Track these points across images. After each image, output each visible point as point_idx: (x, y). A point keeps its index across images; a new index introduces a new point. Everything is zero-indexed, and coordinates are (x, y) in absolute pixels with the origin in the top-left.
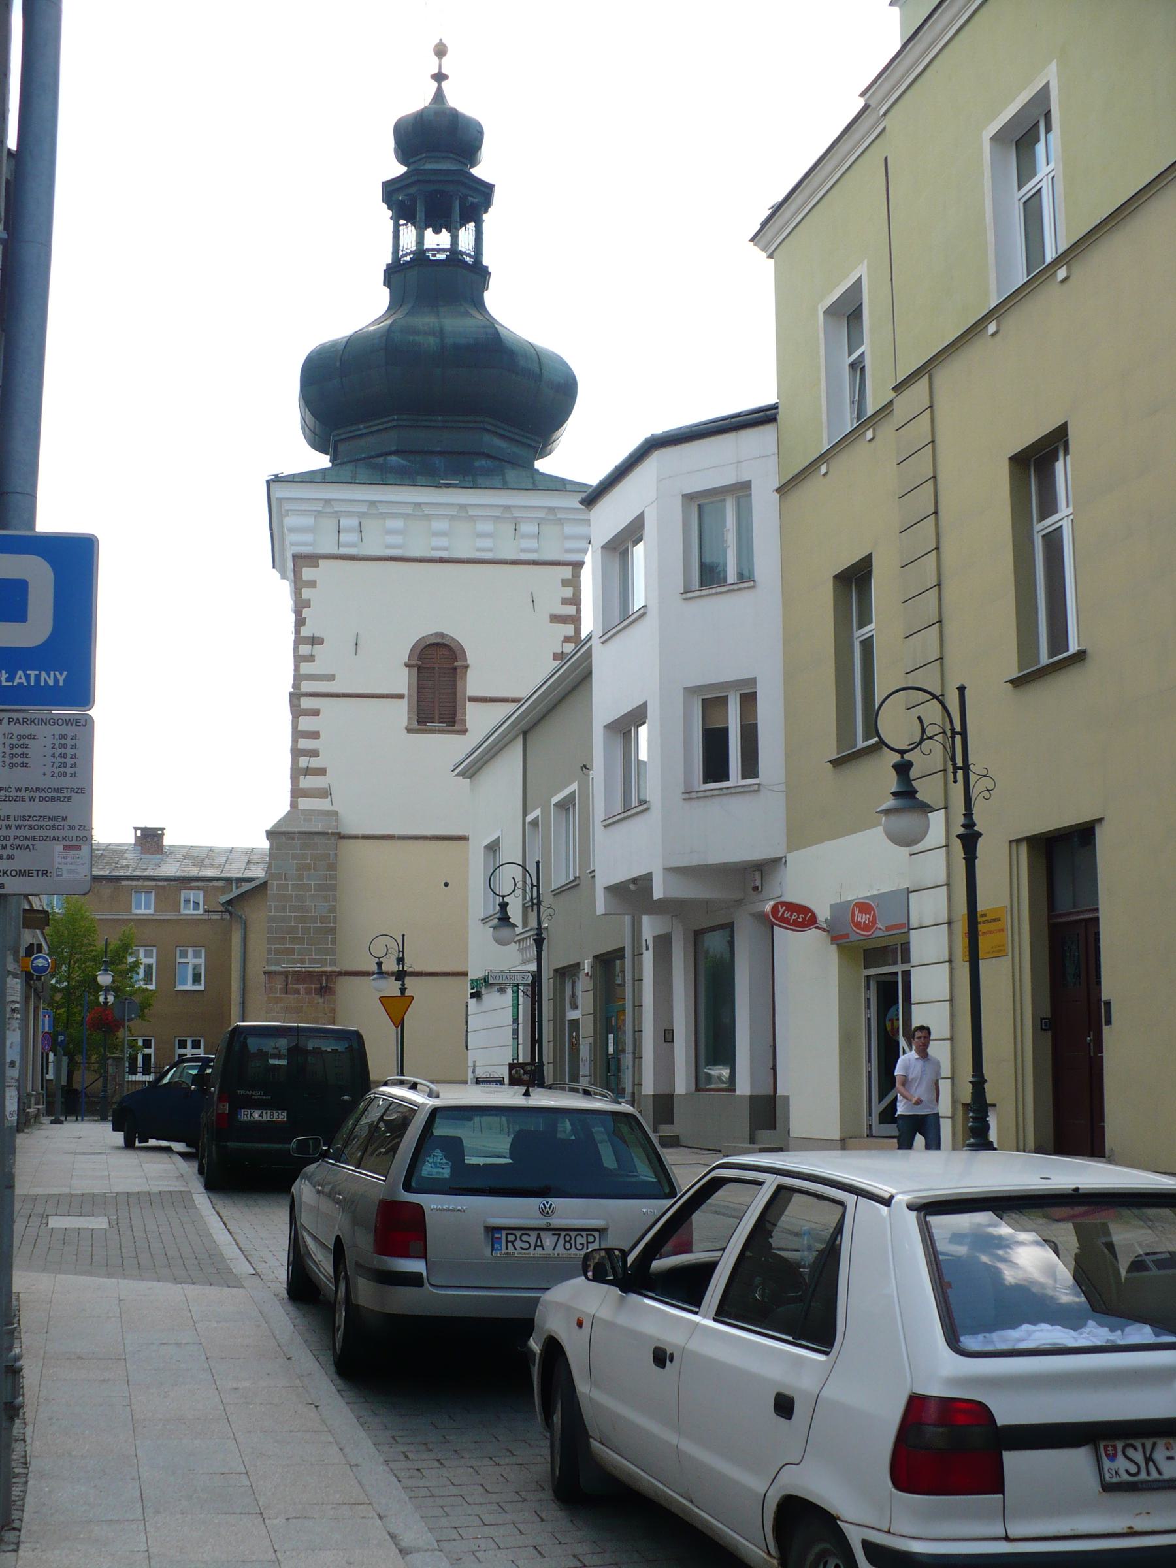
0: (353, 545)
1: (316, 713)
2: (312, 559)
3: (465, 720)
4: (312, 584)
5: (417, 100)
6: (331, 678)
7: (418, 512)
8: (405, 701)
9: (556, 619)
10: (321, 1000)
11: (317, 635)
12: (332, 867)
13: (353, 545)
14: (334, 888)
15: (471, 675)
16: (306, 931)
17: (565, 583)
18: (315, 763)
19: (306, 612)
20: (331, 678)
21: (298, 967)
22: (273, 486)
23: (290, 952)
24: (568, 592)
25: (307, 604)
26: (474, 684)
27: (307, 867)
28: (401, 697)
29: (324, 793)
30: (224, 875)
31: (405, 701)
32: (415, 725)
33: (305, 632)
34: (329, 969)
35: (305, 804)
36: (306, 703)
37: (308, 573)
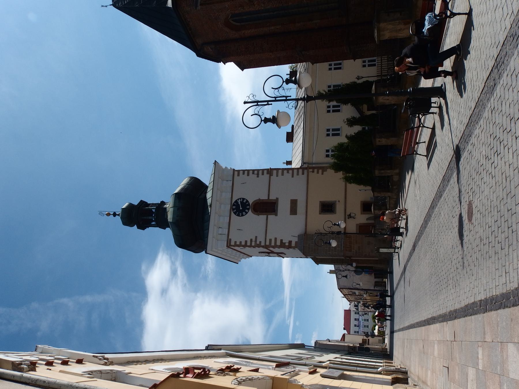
5: (118, 218)
9: (248, 175)
26: (264, 197)
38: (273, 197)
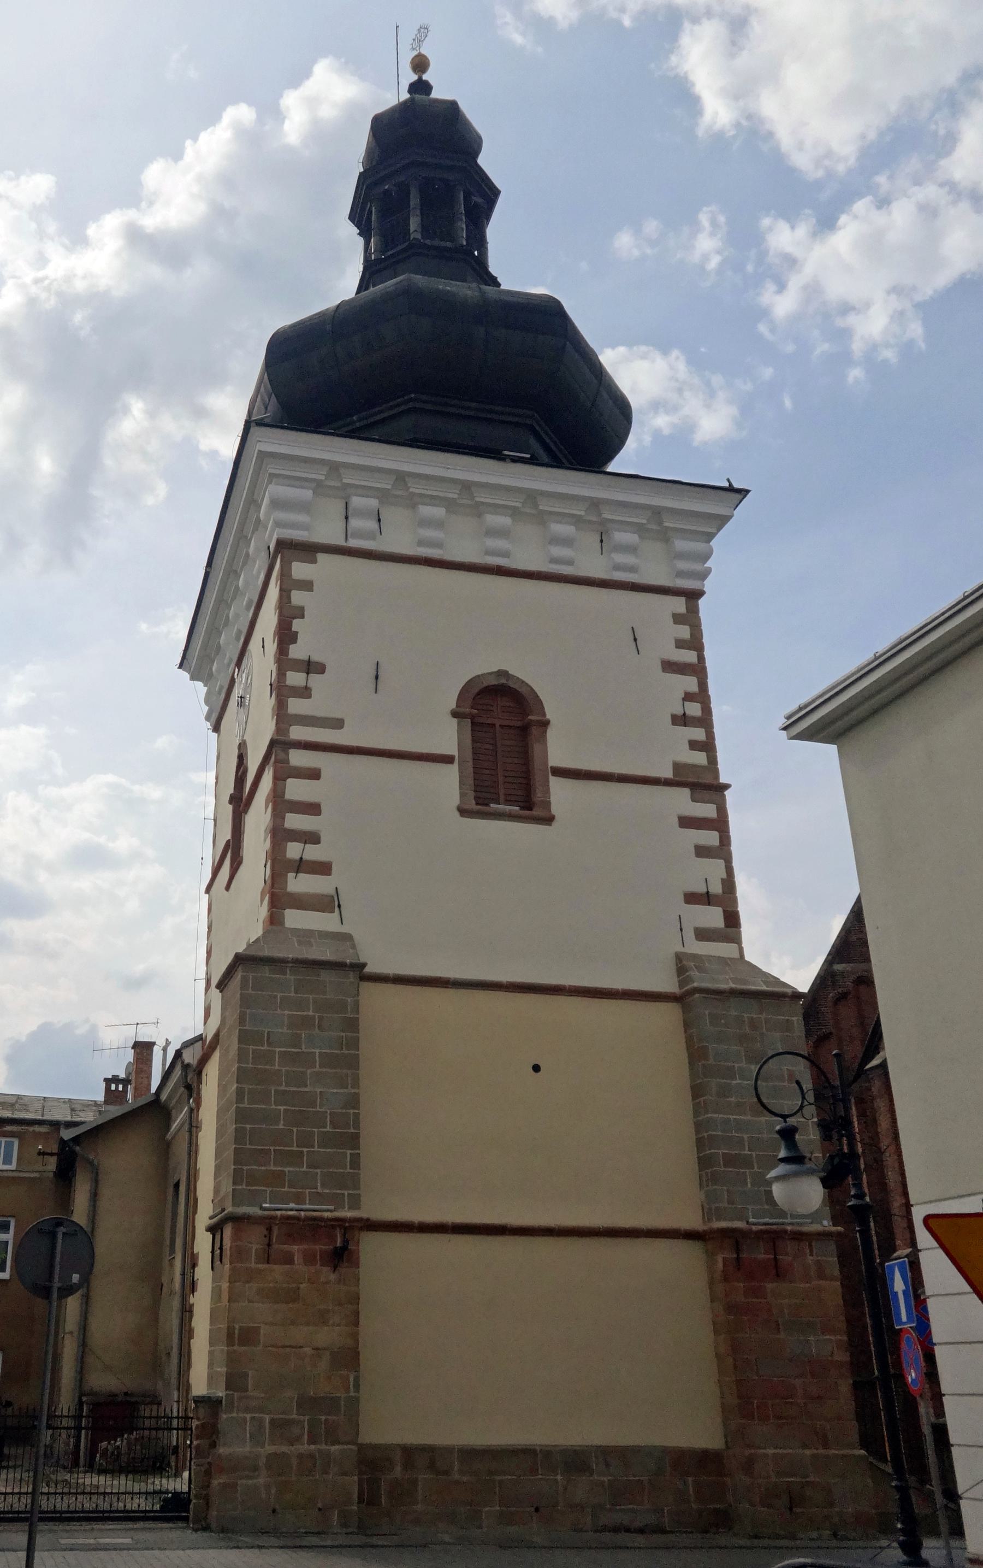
0: (370, 536)
1: (314, 774)
2: (309, 551)
3: (549, 803)
4: (307, 586)
6: (338, 724)
7: (467, 500)
8: (454, 768)
9: (669, 666)
10: (333, 1277)
11: (315, 658)
12: (352, 1025)
13: (370, 536)
14: (353, 1063)
15: (551, 734)
16: (305, 1140)
17: (678, 619)
18: (312, 853)
19: (297, 625)
20: (338, 724)
21: (291, 1208)
22: (254, 430)
23: (278, 1178)
24: (684, 632)
25: (300, 613)
26: (558, 749)
27: (306, 1022)
28: (448, 760)
29: (328, 903)
30: (47, 1117)
31: (454, 768)
32: (472, 805)
33: (297, 652)
34: (348, 1214)
35: (294, 919)
36: (298, 758)
37: (300, 570)
38: (560, 793)
